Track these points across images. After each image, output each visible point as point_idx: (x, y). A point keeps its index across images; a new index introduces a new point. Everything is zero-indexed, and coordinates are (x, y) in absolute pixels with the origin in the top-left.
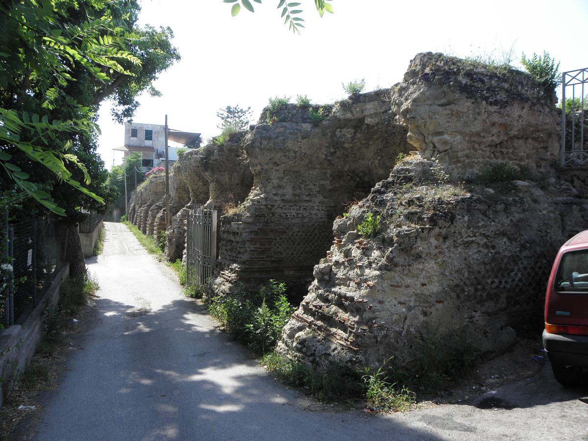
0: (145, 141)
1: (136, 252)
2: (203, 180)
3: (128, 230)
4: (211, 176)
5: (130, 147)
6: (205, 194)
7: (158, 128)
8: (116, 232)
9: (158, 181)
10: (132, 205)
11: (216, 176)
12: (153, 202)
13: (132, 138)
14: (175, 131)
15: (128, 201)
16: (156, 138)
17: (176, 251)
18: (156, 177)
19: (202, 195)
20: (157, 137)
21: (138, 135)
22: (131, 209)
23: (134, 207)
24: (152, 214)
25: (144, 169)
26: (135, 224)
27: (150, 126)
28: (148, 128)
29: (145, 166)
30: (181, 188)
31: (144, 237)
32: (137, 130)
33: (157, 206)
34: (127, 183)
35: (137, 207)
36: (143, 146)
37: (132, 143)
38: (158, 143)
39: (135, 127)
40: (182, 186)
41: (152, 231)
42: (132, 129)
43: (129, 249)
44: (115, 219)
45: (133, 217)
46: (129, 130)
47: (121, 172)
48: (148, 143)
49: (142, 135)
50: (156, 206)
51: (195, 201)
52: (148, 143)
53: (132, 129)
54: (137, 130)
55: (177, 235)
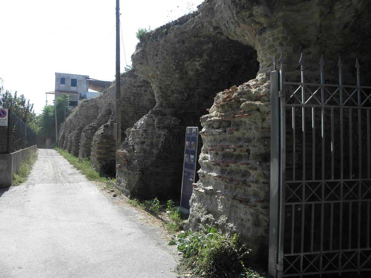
0: (71, 87)
1: (71, 178)
2: (181, 70)
3: (59, 154)
4: (266, 16)
5: (58, 92)
6: (180, 94)
7: (81, 77)
8: (48, 155)
9: (90, 105)
10: (62, 134)
11: (280, 14)
12: (233, 14)
13: (61, 85)
14: (92, 80)
15: (58, 132)
16: (79, 85)
17: (140, 179)
18: (86, 101)
19: (175, 95)
20: (80, 84)
21: (66, 83)
22: (60, 137)
23: (64, 135)
24: (85, 135)
25: (70, 108)
26: (65, 148)
27: (75, 76)
28: (74, 77)
29: (71, 106)
30: (126, 99)
31: (77, 159)
32: (65, 78)
33: (91, 126)
34: (57, 117)
35: (66, 135)
36: (70, 91)
37: (61, 89)
38: (81, 88)
39: (63, 76)
40: (127, 98)
41: (88, 155)
42: (61, 78)
43: (62, 174)
44: (48, 146)
45: (63, 143)
46: (59, 79)
47: (52, 110)
48: (73, 89)
49: (68, 83)
50: (90, 126)
51: (164, 105)
52: (73, 89)
53: (61, 78)
54: (65, 78)
55: (141, 155)
